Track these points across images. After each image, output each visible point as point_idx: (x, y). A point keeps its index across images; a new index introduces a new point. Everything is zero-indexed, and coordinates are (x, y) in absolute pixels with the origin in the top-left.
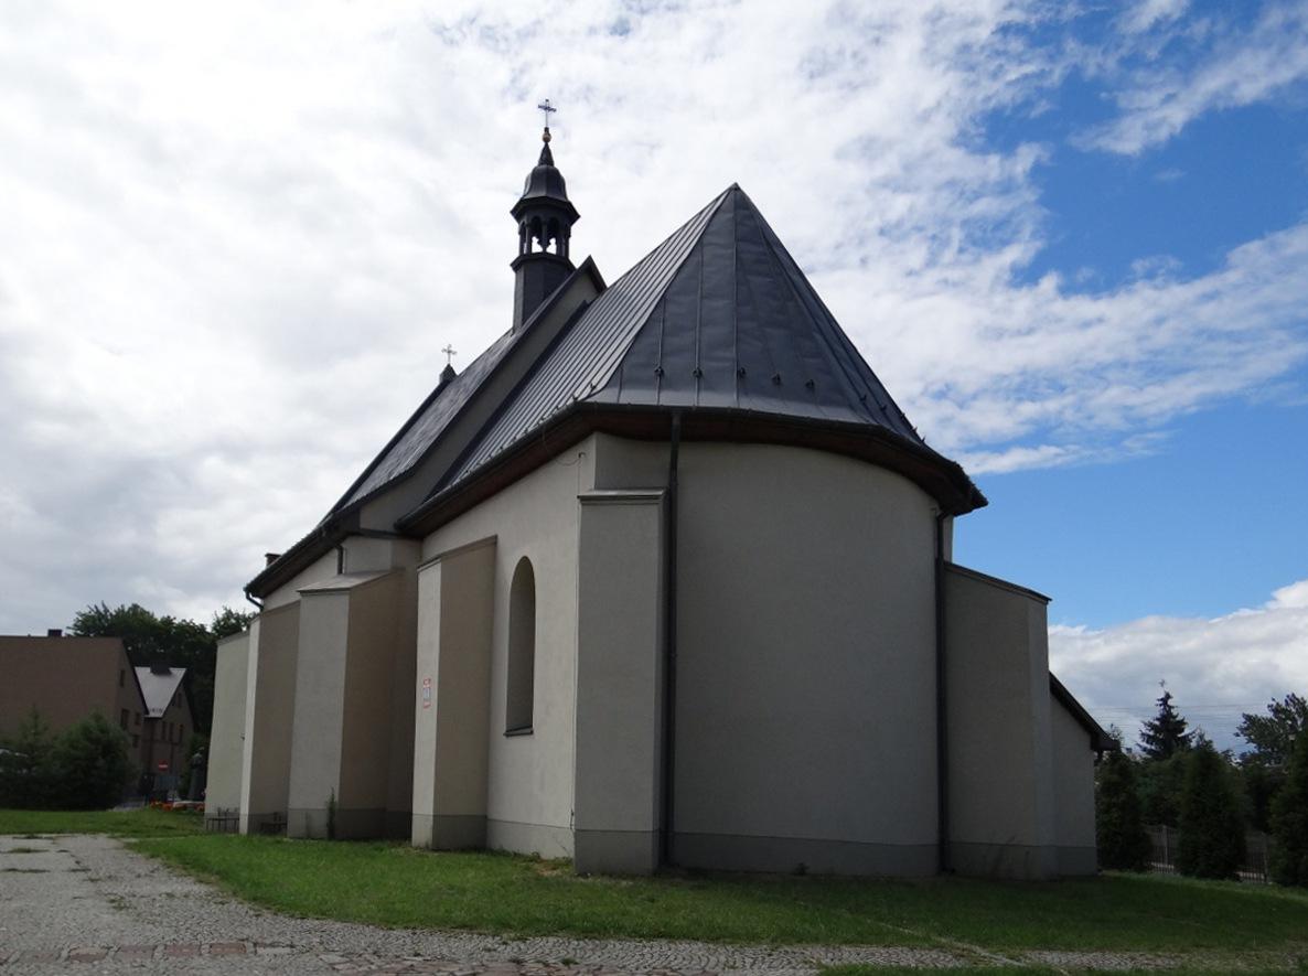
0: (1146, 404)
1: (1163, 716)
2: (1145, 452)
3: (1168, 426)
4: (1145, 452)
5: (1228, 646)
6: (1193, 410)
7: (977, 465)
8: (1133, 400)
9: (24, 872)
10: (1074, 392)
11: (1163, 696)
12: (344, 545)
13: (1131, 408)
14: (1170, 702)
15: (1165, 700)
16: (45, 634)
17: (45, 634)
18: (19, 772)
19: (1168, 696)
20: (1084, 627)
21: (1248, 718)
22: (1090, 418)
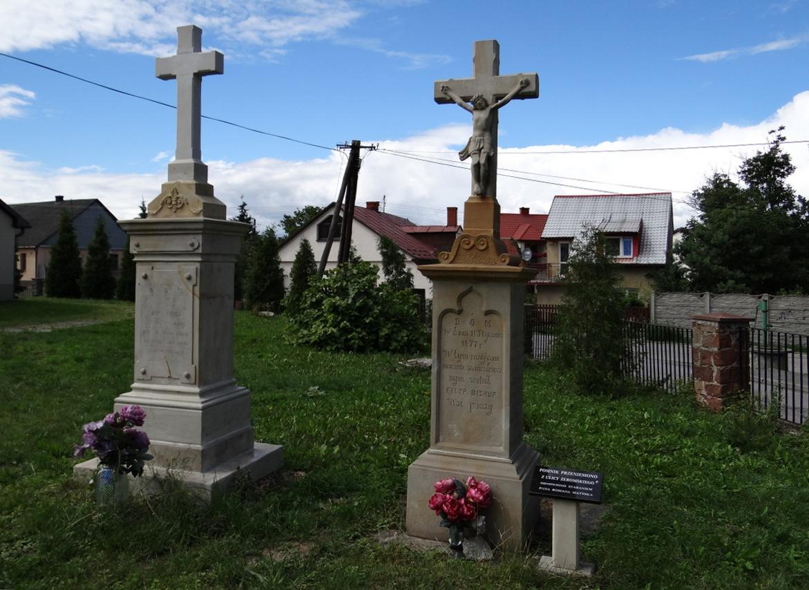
0: (272, 31)
1: (241, 216)
2: (274, 61)
3: (284, 47)
4: (274, 61)
5: (303, 178)
6: (299, 39)
7: (169, 52)
8: (265, 26)
9: (457, 251)
10: (228, 15)
11: (241, 204)
12: (442, 220)
13: (264, 32)
14: (245, 208)
15: (242, 207)
16: (54, 200)
17: (54, 200)
18: (263, 247)
19: (245, 204)
20: (232, 163)
21: (286, 217)
22: (239, 33)
